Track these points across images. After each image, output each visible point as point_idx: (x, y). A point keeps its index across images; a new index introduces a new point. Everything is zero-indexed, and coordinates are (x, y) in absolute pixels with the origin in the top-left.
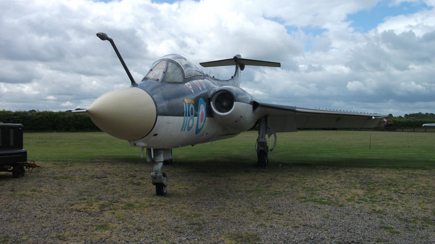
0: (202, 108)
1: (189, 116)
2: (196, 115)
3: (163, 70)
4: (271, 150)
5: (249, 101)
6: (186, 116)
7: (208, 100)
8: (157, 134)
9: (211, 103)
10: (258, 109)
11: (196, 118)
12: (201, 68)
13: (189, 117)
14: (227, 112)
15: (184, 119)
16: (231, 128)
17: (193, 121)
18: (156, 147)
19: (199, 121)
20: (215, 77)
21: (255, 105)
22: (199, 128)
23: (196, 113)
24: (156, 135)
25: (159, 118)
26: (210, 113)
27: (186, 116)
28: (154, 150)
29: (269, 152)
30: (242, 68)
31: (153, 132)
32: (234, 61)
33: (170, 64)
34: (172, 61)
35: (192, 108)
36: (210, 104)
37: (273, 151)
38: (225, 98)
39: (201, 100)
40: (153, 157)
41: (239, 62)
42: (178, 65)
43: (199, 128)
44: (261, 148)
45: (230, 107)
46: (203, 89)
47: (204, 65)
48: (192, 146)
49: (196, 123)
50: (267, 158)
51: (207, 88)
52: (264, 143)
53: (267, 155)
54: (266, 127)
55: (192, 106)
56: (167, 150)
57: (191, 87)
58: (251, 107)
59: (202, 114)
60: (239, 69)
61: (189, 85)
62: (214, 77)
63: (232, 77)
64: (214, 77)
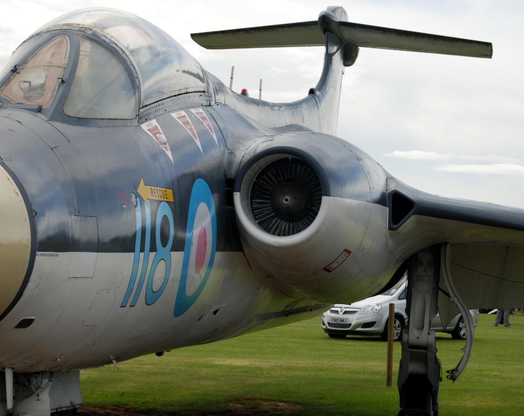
0: (204, 218)
1: (153, 248)
2: (179, 245)
3: (58, 73)
4: (453, 375)
5: (377, 194)
6: (142, 250)
7: (224, 184)
8: (30, 321)
9: (237, 197)
10: (410, 222)
11: (177, 256)
12: (196, 50)
13: (153, 254)
14: (267, 230)
15: (136, 261)
16: (301, 287)
17: (164, 269)
18: (21, 367)
19: (193, 269)
20: (253, 94)
21: (399, 205)
22: (190, 291)
23: (180, 234)
24: (26, 323)
25: (43, 260)
26: (229, 234)
27: (153, 248)
28: (16, 376)
29: (445, 386)
30: (349, 58)
31: (19, 313)
32: (318, 31)
33: (86, 47)
34: (95, 38)
35: (165, 218)
36: (230, 202)
37: (462, 377)
38: (290, 181)
39: (200, 186)
40: (10, 404)
41: (339, 37)
42: (112, 49)
43: (190, 291)
44: (414, 367)
45: (306, 213)
46: (208, 144)
47: (208, 40)
48: (159, 354)
49: (177, 286)
50: (435, 404)
51: (223, 138)
52: (425, 348)
53: (434, 395)
54: (437, 289)
55: (165, 210)
56: (61, 371)
57: (163, 137)
58: (382, 215)
59: (203, 235)
60: (337, 59)
61: (155, 131)
62: (244, 92)
63: (312, 92)
64: (244, 92)
